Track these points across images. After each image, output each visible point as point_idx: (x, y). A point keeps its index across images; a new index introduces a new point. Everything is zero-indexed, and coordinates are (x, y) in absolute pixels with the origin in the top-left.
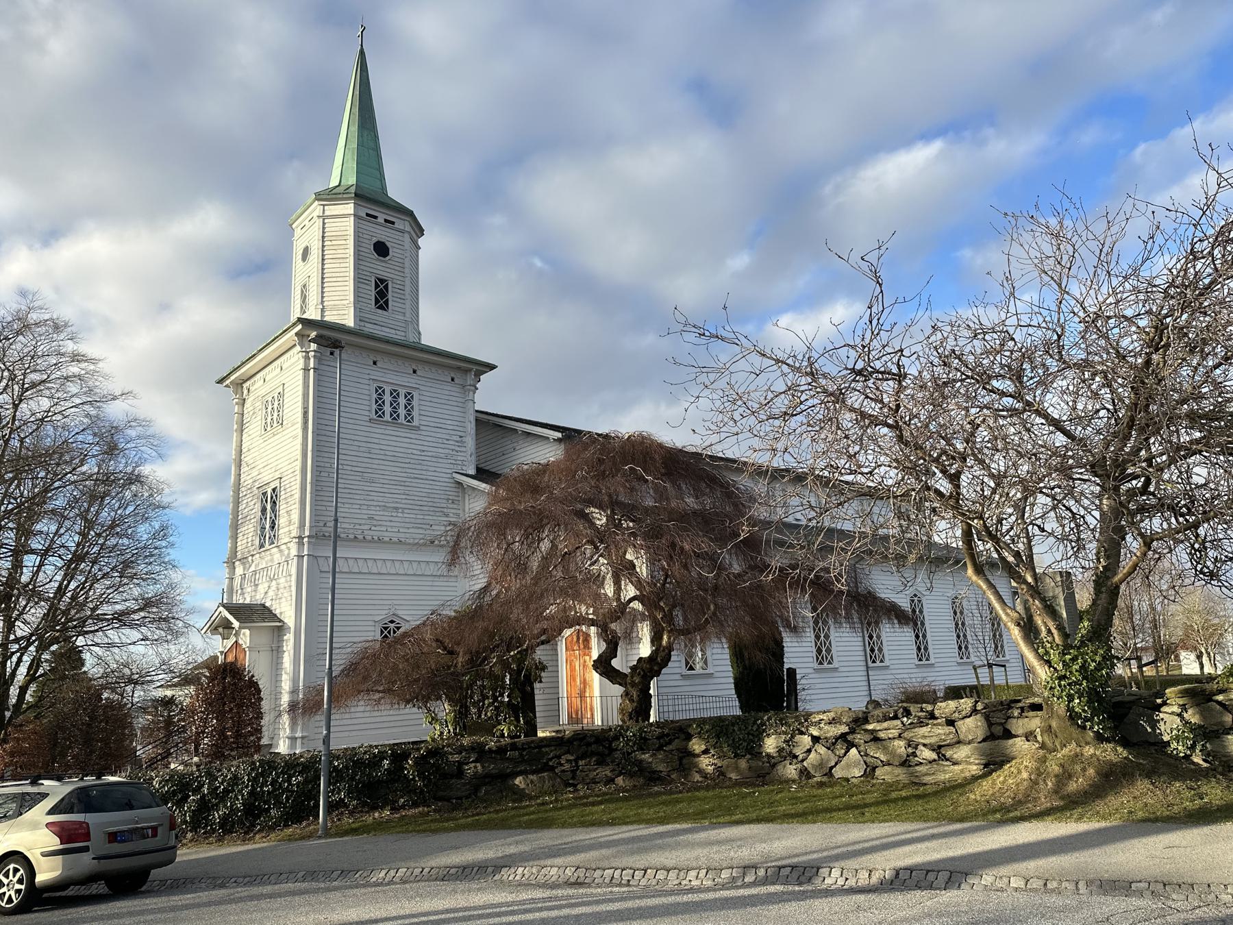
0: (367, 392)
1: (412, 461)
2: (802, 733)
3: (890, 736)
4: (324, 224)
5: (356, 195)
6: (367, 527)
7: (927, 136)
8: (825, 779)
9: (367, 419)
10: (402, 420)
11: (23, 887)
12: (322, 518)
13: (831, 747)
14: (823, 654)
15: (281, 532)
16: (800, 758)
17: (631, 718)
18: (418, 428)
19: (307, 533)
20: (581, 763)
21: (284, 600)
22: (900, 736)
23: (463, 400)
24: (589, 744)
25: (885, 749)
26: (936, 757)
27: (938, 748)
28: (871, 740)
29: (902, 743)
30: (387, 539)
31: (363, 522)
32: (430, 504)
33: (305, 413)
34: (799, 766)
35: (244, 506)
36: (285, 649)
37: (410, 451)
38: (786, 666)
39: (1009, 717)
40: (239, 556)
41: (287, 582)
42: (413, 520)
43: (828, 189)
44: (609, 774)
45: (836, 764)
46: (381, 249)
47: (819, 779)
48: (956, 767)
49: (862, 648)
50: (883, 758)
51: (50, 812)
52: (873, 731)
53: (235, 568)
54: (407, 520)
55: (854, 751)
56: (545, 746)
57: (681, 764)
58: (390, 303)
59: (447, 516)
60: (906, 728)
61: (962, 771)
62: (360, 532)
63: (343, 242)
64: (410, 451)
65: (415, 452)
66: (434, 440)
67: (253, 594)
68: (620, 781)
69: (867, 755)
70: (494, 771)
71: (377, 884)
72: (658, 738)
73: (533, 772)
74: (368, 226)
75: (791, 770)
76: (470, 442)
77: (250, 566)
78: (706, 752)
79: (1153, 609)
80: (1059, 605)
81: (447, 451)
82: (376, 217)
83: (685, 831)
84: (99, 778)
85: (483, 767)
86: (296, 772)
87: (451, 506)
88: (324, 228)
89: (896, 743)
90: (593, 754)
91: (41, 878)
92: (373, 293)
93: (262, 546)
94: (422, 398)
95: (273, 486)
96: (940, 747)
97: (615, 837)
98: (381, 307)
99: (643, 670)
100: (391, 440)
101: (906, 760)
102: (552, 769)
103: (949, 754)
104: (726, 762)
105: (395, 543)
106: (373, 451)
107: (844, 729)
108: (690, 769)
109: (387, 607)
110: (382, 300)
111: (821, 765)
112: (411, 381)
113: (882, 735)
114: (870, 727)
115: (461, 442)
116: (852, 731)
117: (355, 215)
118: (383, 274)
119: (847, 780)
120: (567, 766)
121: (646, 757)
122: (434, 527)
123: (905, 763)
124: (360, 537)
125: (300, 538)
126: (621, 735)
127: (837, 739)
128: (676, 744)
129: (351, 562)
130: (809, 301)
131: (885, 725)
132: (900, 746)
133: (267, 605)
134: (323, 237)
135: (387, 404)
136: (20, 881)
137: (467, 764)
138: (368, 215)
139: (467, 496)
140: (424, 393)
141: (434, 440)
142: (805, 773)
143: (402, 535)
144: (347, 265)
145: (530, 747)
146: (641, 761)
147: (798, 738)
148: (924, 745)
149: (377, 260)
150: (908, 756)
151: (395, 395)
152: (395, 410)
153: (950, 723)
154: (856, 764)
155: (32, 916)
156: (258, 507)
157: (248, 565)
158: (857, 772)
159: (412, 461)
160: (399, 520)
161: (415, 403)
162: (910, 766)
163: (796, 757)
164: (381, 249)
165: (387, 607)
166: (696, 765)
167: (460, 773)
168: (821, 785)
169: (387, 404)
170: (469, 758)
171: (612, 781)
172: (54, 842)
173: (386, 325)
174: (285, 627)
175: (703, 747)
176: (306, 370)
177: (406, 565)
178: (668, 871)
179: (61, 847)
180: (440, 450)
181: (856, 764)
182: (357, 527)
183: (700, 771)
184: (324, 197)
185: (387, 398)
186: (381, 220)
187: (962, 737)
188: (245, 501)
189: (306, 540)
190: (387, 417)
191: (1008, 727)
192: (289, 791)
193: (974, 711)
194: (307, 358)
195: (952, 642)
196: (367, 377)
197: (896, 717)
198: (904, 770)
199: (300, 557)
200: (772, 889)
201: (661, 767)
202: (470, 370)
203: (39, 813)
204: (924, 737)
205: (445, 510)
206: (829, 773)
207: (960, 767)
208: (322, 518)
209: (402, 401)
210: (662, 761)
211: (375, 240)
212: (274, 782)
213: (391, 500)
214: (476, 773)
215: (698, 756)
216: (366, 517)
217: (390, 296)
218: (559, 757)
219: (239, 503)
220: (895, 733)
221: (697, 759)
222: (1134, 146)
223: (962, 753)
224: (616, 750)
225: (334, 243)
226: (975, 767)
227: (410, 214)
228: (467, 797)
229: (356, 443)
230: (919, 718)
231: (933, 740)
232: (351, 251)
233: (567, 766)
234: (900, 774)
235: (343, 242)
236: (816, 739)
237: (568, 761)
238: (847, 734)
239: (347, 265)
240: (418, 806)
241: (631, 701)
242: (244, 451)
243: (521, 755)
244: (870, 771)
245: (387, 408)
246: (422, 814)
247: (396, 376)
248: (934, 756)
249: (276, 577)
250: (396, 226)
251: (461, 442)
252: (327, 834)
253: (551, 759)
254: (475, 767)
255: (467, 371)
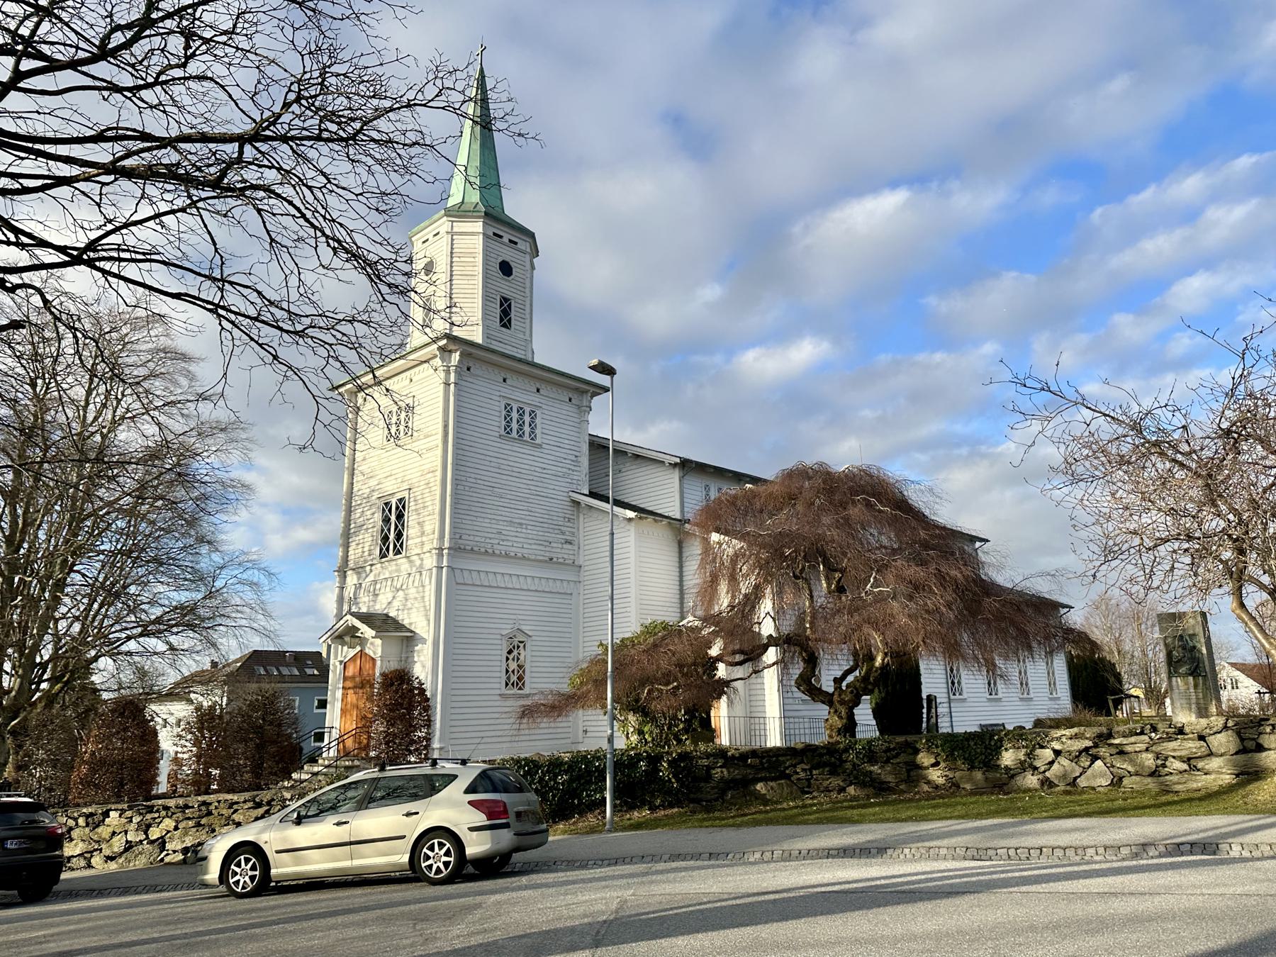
0: (497, 409)
1: (535, 478)
2: (1042, 747)
3: (1138, 749)
4: (452, 240)
5: (486, 214)
6: (497, 541)
7: (894, 185)
8: (1068, 788)
9: (497, 434)
10: (526, 437)
11: (452, 859)
12: (458, 531)
13: (1076, 758)
14: (954, 686)
15: (409, 542)
16: (1042, 769)
17: (839, 734)
18: (540, 446)
19: (447, 545)
20: (814, 772)
21: (414, 610)
22: (1147, 750)
23: (578, 421)
24: (821, 755)
25: (1132, 761)
26: (1187, 768)
27: (1188, 760)
28: (1117, 753)
29: (1150, 756)
30: (513, 554)
31: (493, 536)
32: (550, 521)
33: (446, 426)
34: (1041, 777)
35: (358, 515)
36: (416, 659)
37: (533, 468)
38: (924, 696)
39: (1261, 733)
40: (351, 564)
41: (418, 592)
42: (535, 537)
43: (797, 229)
44: (841, 784)
45: (1081, 774)
46: (506, 268)
47: (1063, 788)
48: (1208, 776)
49: (945, 681)
50: (1130, 768)
51: (467, 791)
52: (1117, 745)
53: (345, 577)
54: (530, 536)
55: (1099, 763)
56: (783, 755)
57: (909, 776)
58: (513, 322)
59: (563, 533)
60: (1153, 743)
61: (1215, 780)
62: (490, 546)
63: (472, 260)
64: (533, 468)
65: (537, 469)
66: (553, 458)
67: (371, 603)
68: (851, 790)
69: (1113, 766)
70: (738, 777)
71: (751, 863)
72: (885, 752)
73: (773, 779)
74: (495, 245)
75: (1031, 780)
76: (585, 461)
77: (367, 576)
78: (936, 764)
79: (1145, 655)
80: (1199, 642)
81: (564, 470)
82: (501, 237)
83: (1013, 825)
84: (382, 769)
85: (729, 772)
86: (560, 771)
87: (568, 524)
88: (452, 244)
89: (1144, 755)
90: (825, 765)
91: (470, 851)
92: (498, 311)
93: (383, 556)
94: (545, 416)
95: (399, 496)
96: (1189, 759)
97: (953, 828)
98: (504, 326)
99: (856, 689)
100: (519, 455)
101: (1156, 771)
102: (788, 777)
103: (1200, 765)
104: (958, 774)
105: (520, 558)
106: (502, 467)
107: (1089, 743)
108: (918, 781)
109: (512, 622)
110: (505, 319)
111: (1064, 776)
112: (534, 399)
113: (1129, 749)
114: (1117, 741)
115: (576, 461)
116: (1096, 746)
117: (484, 234)
118: (508, 294)
119: (1094, 789)
120: (802, 775)
121: (875, 768)
122: (553, 545)
123: (1154, 774)
124: (490, 551)
125: (441, 549)
126: (850, 747)
127: (1080, 752)
128: (902, 758)
129: (466, 574)
130: (781, 336)
131: (1133, 739)
132: (1149, 760)
133: (391, 615)
134: (452, 253)
135: (515, 421)
136: (447, 854)
137: (714, 769)
138: (495, 234)
139: (581, 516)
140: (546, 412)
141: (553, 458)
142: (1047, 783)
143: (525, 551)
144: (476, 282)
145: (769, 756)
146: (871, 772)
147: (1038, 751)
148: (1174, 757)
149: (503, 279)
150: (1157, 767)
151: (521, 412)
152: (521, 426)
153: (1202, 738)
154: (1102, 775)
155: (455, 886)
156: (378, 517)
157: (364, 575)
158: (1105, 782)
159: (535, 478)
160: (523, 535)
161: (538, 421)
162: (1160, 776)
163: (1036, 768)
164: (506, 268)
165: (512, 622)
166: (925, 777)
167: (708, 777)
168: (1067, 793)
169: (515, 421)
170: (717, 763)
171: (842, 790)
172: (480, 818)
173: (508, 343)
174: (417, 637)
175: (933, 761)
176: (447, 384)
177: (565, 584)
178: (1065, 849)
179: (488, 823)
180: (560, 469)
181: (1102, 775)
182: (488, 541)
183: (928, 782)
184: (455, 213)
185: (515, 415)
186: (505, 240)
187: (1214, 750)
188: (360, 511)
189: (445, 551)
190: (514, 434)
191: (1261, 741)
192: (556, 789)
193: (1226, 727)
194: (448, 372)
195: (928, 685)
196: (498, 393)
197: (1142, 733)
198: (1155, 779)
199: (440, 568)
200: (1164, 860)
201: (890, 778)
202: (587, 392)
203: (455, 791)
204: (1174, 750)
205: (562, 528)
206: (1074, 783)
207: (1213, 777)
208: (458, 531)
209: (527, 419)
210: (890, 773)
211: (500, 259)
212: (541, 779)
213: (517, 516)
214: (722, 778)
215: (927, 768)
216: (495, 531)
217: (512, 315)
218: (795, 766)
219: (351, 512)
220: (1143, 746)
221: (926, 772)
222: (1092, 210)
223: (1215, 763)
224: (846, 761)
225: (462, 259)
226: (1228, 777)
227: (532, 235)
228: (716, 800)
229: (488, 458)
230: (1167, 733)
231: (1183, 753)
232: (480, 269)
233: (802, 775)
234: (1150, 783)
235: (472, 260)
236: (1057, 753)
237: (804, 770)
238: (1091, 747)
239: (476, 282)
240: (673, 808)
241: (840, 717)
242: (357, 460)
243: (761, 763)
244: (1117, 781)
245: (515, 426)
246: (680, 814)
247: (522, 394)
248: (1185, 766)
249: (404, 587)
250: (519, 246)
251: (576, 461)
252: (615, 828)
253: (787, 768)
254: (722, 772)
255: (584, 392)
